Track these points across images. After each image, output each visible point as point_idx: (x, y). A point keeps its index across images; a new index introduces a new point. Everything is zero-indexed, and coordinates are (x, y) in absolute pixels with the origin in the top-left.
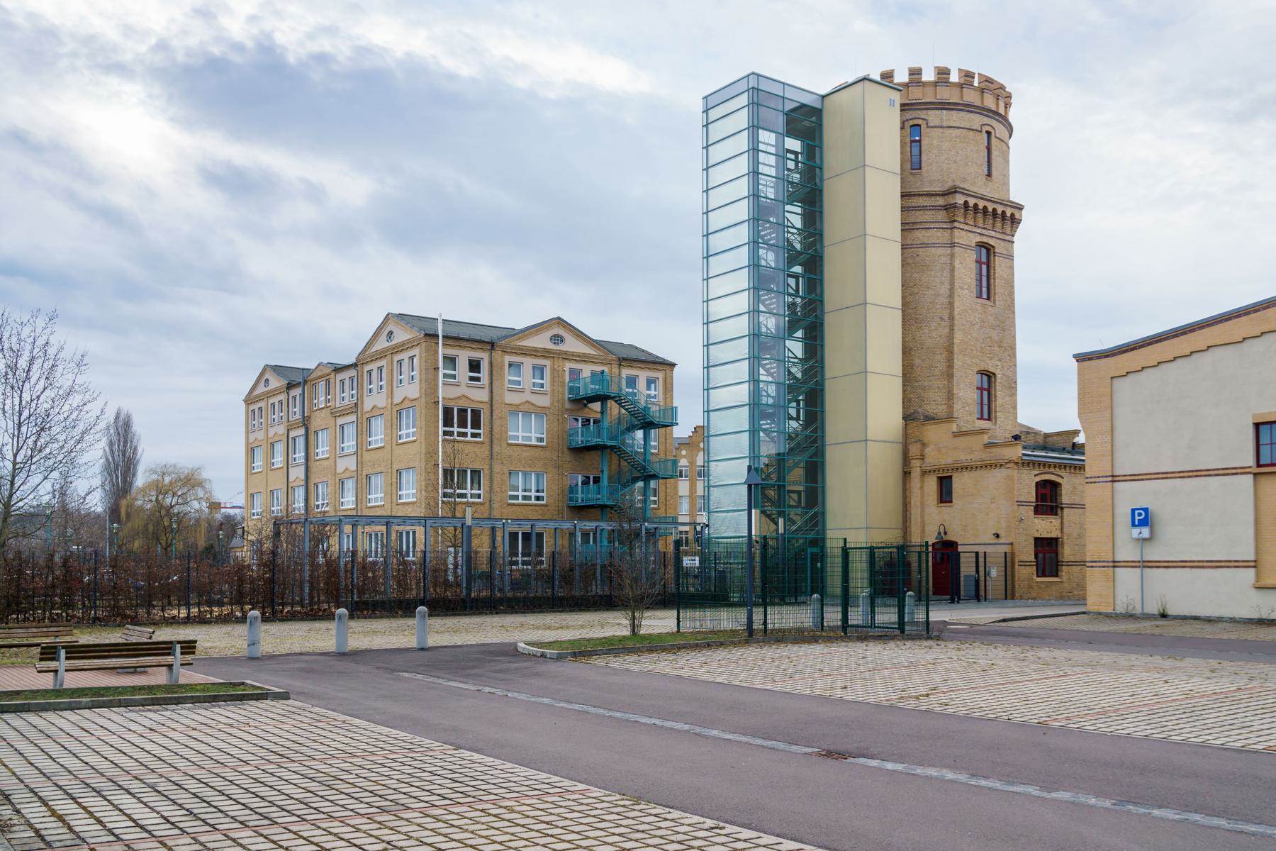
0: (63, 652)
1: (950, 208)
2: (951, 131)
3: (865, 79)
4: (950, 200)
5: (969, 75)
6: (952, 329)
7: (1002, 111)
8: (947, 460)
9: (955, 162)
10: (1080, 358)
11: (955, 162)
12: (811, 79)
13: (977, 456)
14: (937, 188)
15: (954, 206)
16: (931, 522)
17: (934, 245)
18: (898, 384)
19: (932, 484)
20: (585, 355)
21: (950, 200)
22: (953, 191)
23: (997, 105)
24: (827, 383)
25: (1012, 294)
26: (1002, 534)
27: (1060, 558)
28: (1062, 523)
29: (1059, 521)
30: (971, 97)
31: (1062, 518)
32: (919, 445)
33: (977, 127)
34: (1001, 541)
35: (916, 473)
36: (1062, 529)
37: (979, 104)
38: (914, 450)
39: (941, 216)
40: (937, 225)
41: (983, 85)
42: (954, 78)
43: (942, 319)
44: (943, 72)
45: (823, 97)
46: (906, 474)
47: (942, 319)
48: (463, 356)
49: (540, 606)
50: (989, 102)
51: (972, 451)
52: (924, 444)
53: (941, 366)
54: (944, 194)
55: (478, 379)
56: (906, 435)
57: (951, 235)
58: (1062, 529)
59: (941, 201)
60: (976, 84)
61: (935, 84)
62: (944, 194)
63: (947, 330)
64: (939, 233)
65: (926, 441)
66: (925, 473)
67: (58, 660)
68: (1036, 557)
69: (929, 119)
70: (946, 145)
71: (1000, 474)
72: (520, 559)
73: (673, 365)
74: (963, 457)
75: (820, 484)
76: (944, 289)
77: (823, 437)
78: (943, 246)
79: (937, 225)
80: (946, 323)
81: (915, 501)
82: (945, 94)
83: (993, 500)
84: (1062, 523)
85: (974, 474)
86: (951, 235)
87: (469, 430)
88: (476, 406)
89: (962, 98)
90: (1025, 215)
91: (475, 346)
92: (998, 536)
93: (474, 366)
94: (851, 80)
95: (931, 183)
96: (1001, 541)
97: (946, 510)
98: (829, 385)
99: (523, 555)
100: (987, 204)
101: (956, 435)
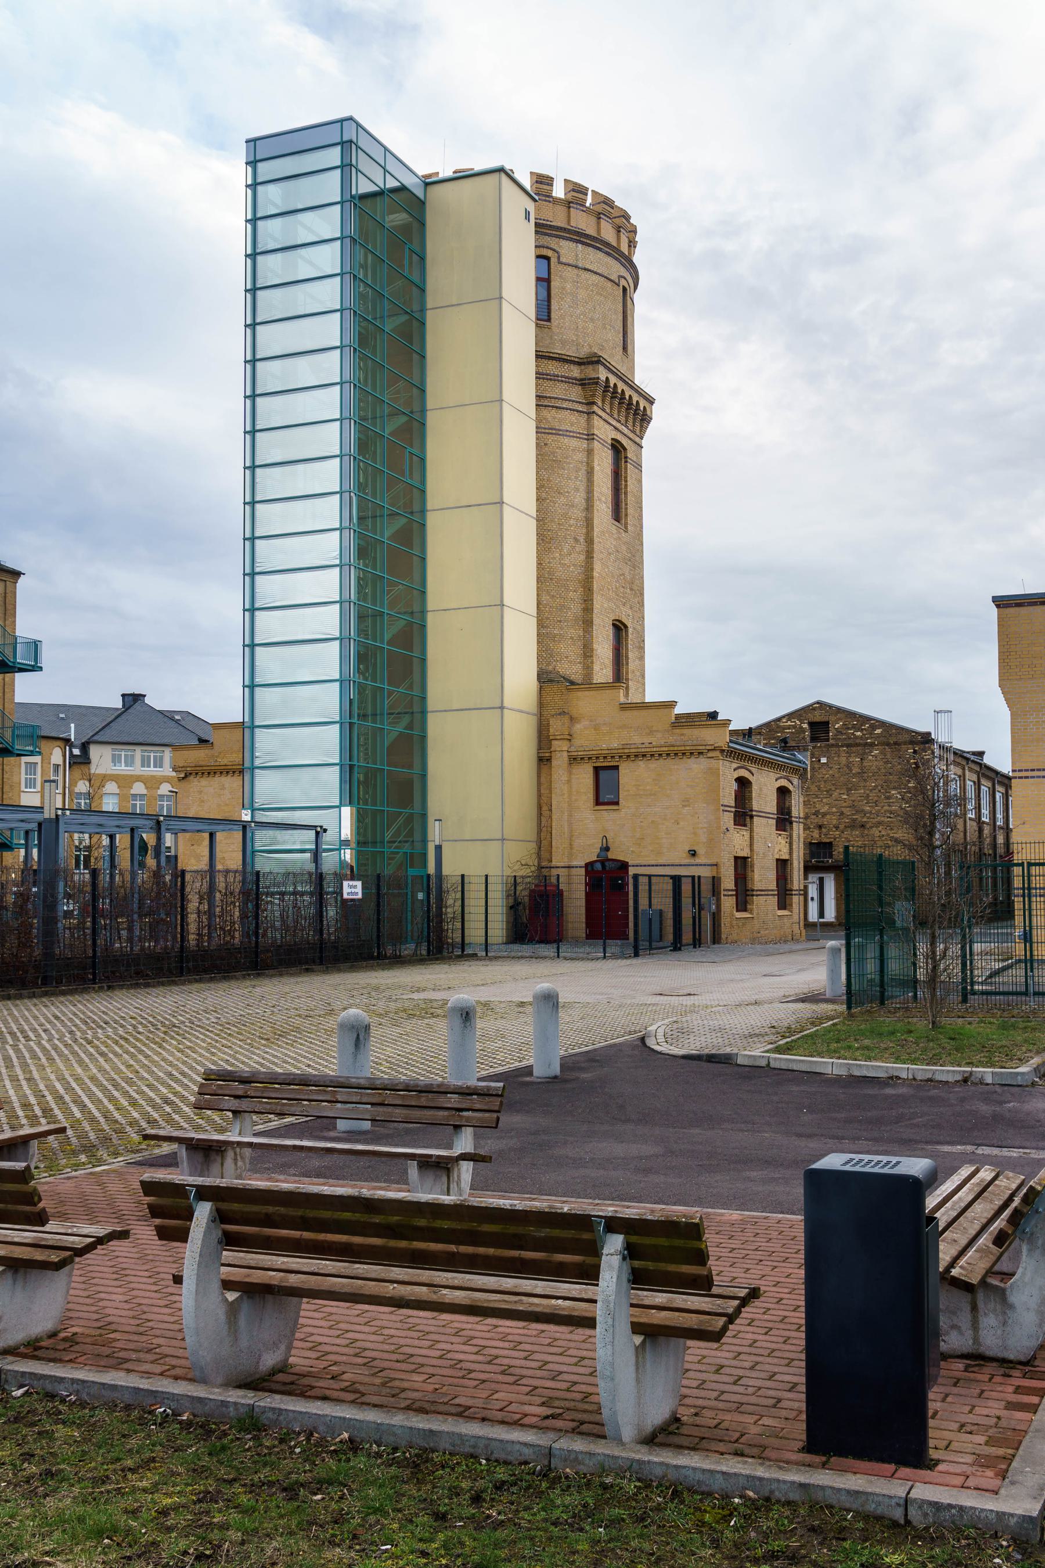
0: (203, 1211)
1: (584, 383)
2: (588, 275)
3: (501, 170)
4: (590, 372)
6: (589, 555)
7: (624, 248)
8: (612, 742)
9: (592, 320)
10: (1002, 602)
11: (592, 320)
12: (419, 148)
13: (659, 740)
14: (571, 352)
15: (596, 381)
16: (583, 834)
17: (567, 434)
18: (533, 622)
19: (585, 776)
21: (590, 372)
22: (594, 360)
24: (430, 618)
25: (641, 516)
26: (701, 851)
27: (789, 887)
28: (751, 838)
29: (747, 834)
30: (582, 222)
31: (751, 831)
32: (566, 719)
33: (614, 277)
34: (698, 861)
35: (560, 761)
36: (751, 845)
38: (557, 726)
39: (575, 393)
40: (570, 405)
41: (599, 208)
42: (559, 191)
43: (576, 540)
45: (427, 184)
46: (543, 760)
47: (576, 540)
49: (139, 974)
50: (608, 233)
51: (651, 732)
52: (571, 718)
53: (575, 608)
54: (581, 363)
56: (541, 704)
57: (589, 421)
58: (751, 845)
59: (575, 372)
62: (581, 363)
63: (582, 557)
64: (574, 417)
65: (574, 713)
66: (574, 760)
67: (590, 1274)
68: (736, 885)
69: (562, 252)
70: (582, 294)
71: (697, 766)
73: (16, 574)
74: (638, 740)
75: (417, 770)
76: (580, 498)
77: (423, 699)
78: (578, 436)
79: (570, 405)
80: (581, 547)
81: (558, 801)
83: (686, 802)
84: (751, 838)
85: (653, 764)
86: (589, 421)
90: (657, 412)
92: (693, 854)
94: (478, 167)
95: (563, 342)
96: (698, 861)
97: (607, 815)
98: (432, 621)
100: (625, 388)
101: (625, 707)
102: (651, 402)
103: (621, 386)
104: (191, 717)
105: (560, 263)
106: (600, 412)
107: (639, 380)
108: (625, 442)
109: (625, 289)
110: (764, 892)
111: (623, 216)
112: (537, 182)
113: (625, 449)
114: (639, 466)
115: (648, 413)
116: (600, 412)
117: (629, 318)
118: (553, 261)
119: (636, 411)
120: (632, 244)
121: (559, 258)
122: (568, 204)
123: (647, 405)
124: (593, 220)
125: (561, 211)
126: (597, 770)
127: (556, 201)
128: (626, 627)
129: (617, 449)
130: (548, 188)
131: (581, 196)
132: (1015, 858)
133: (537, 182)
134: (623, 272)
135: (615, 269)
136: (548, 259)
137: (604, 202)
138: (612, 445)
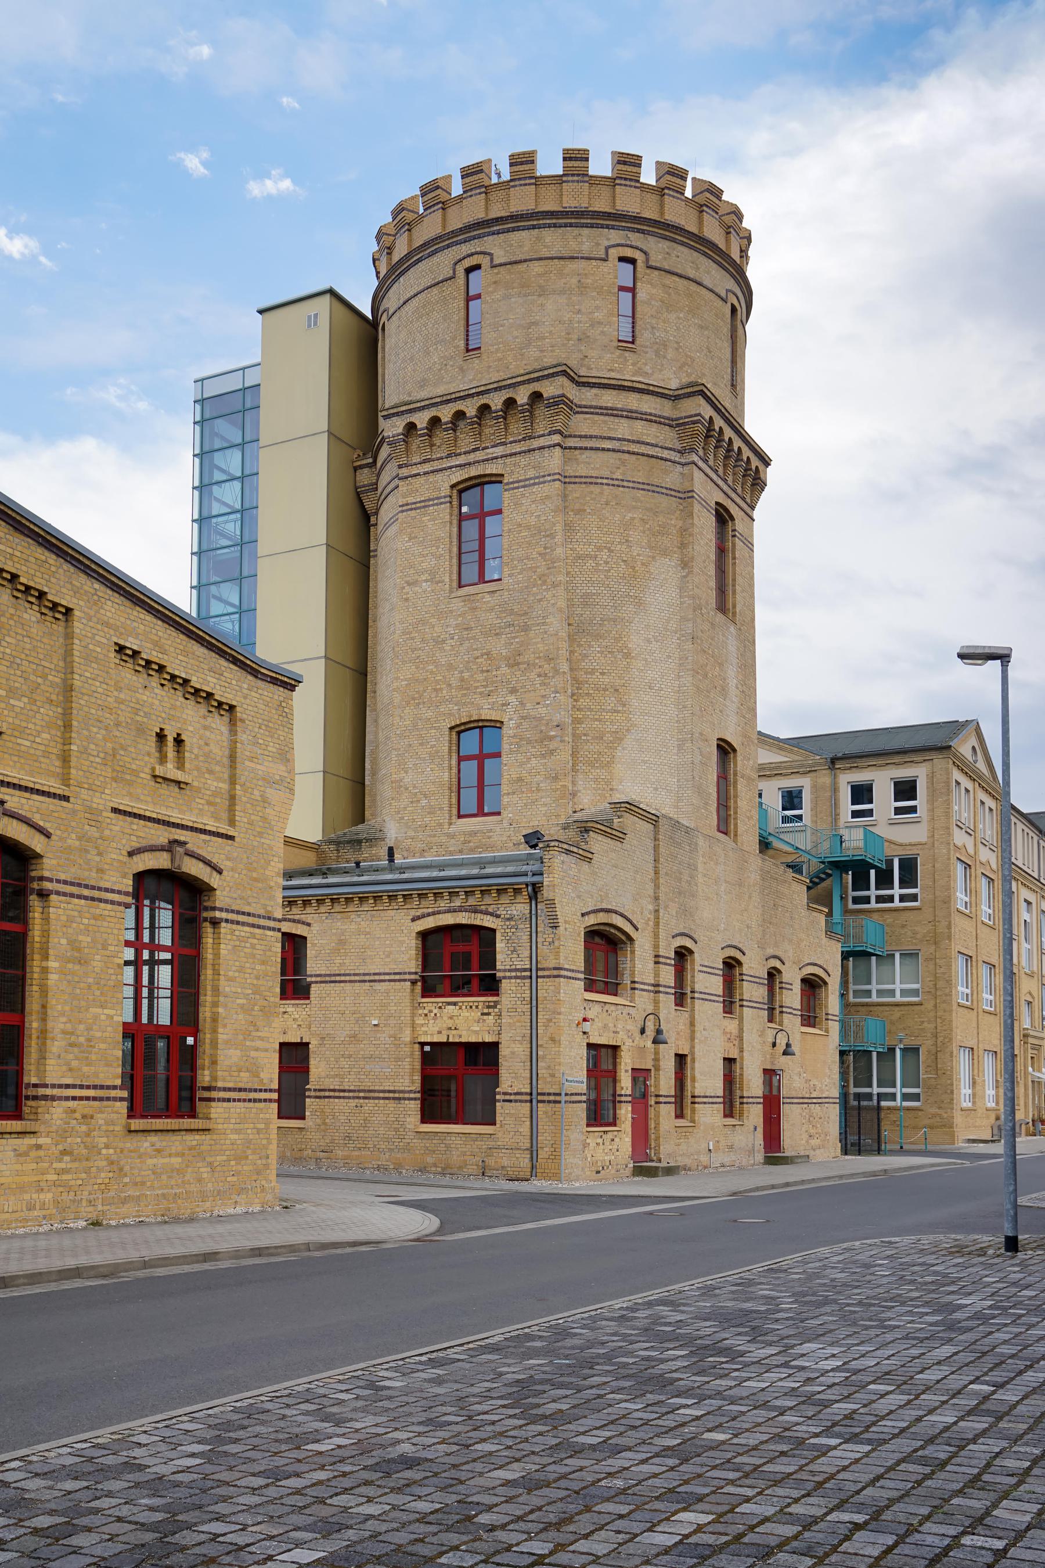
5: (628, 162)
7: (735, 255)
20: (779, 765)
23: (728, 241)
30: (676, 213)
31: (693, 1010)
37: (693, 229)
41: (700, 199)
42: (648, 176)
44: (628, 162)
48: (882, 782)
50: (713, 232)
55: (913, 810)
60: (688, 193)
61: (612, 182)
72: (898, 1090)
82: (628, 202)
87: (897, 891)
88: (908, 852)
89: (662, 213)
90: (771, 474)
91: (897, 759)
93: (905, 790)
99: (904, 1085)
102: (766, 462)
103: (728, 433)
104: (469, 932)
105: (649, 267)
106: (701, 463)
107: (751, 427)
108: (734, 510)
109: (734, 310)
110: (708, 1099)
111: (733, 212)
112: (619, 162)
113: (732, 518)
114: (750, 546)
115: (762, 476)
116: (701, 463)
117: (880, 761)
118: (640, 264)
119: (746, 469)
120: (744, 253)
121: (647, 260)
122: (660, 191)
123: (761, 467)
124: (693, 214)
125: (652, 199)
126: (460, 816)
127: (645, 188)
128: (734, 750)
129: (723, 517)
130: (634, 169)
131: (678, 181)
132: (630, 1109)
133: (619, 162)
134: (731, 284)
135: (724, 283)
136: (632, 261)
137: (708, 190)
138: (716, 510)
